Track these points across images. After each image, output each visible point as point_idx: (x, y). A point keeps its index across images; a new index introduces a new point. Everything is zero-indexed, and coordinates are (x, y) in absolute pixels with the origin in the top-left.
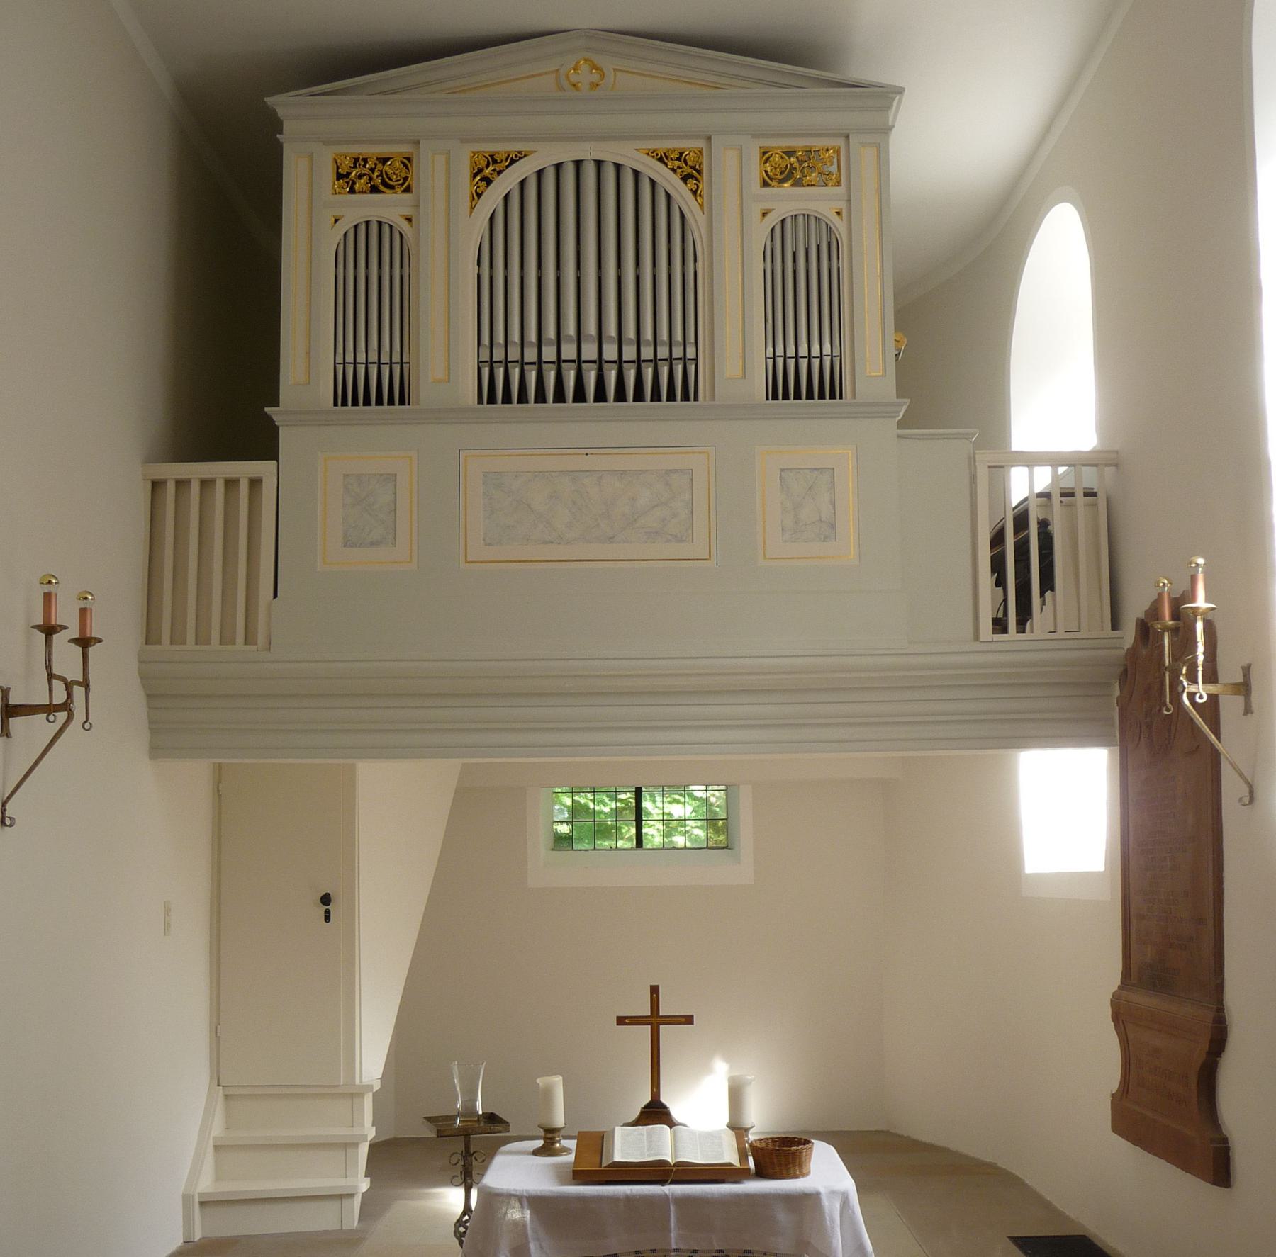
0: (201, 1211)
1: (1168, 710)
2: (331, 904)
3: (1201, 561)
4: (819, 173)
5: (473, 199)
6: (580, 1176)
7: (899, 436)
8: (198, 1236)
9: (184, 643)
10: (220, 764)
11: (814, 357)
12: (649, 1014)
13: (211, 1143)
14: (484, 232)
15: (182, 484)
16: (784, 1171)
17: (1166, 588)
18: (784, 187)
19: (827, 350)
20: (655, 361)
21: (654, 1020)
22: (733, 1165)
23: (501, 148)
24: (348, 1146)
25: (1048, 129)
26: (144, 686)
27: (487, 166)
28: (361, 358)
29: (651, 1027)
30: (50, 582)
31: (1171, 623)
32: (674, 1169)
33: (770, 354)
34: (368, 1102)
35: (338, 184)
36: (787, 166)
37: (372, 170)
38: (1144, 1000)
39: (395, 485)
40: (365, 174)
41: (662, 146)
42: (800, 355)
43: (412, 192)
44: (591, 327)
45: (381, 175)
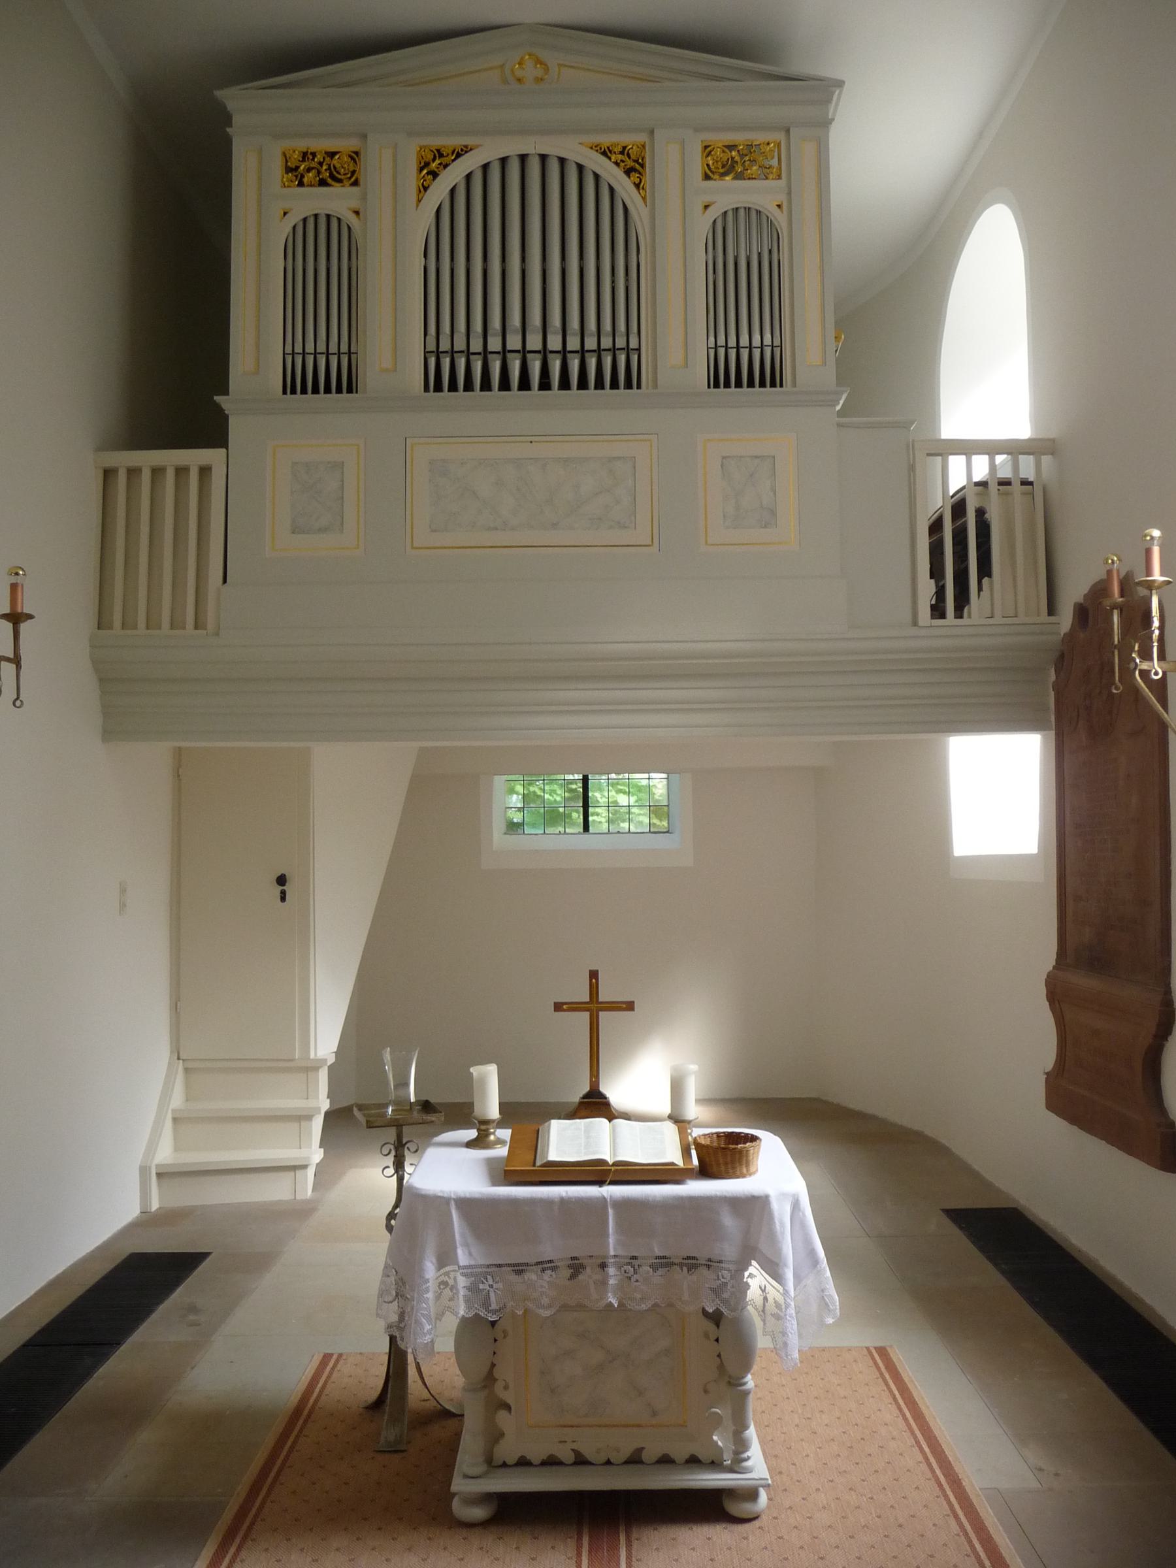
2: (287, 884)
3: (1156, 533)
4: (760, 167)
5: (420, 191)
7: (839, 425)
8: (155, 1206)
10: (179, 748)
11: (755, 347)
13: (169, 1116)
14: (430, 224)
15: (133, 472)
16: (731, 1171)
17: (1115, 565)
18: (725, 180)
19: (767, 340)
20: (599, 351)
21: (594, 1006)
22: (676, 1165)
27: (434, 160)
28: (310, 348)
30: (17, 574)
31: (1121, 599)
32: (613, 1168)
33: (712, 344)
34: (323, 1076)
35: (287, 178)
36: (728, 159)
37: (321, 164)
39: (343, 473)
40: (313, 168)
41: (606, 140)
43: (360, 185)
45: (329, 168)
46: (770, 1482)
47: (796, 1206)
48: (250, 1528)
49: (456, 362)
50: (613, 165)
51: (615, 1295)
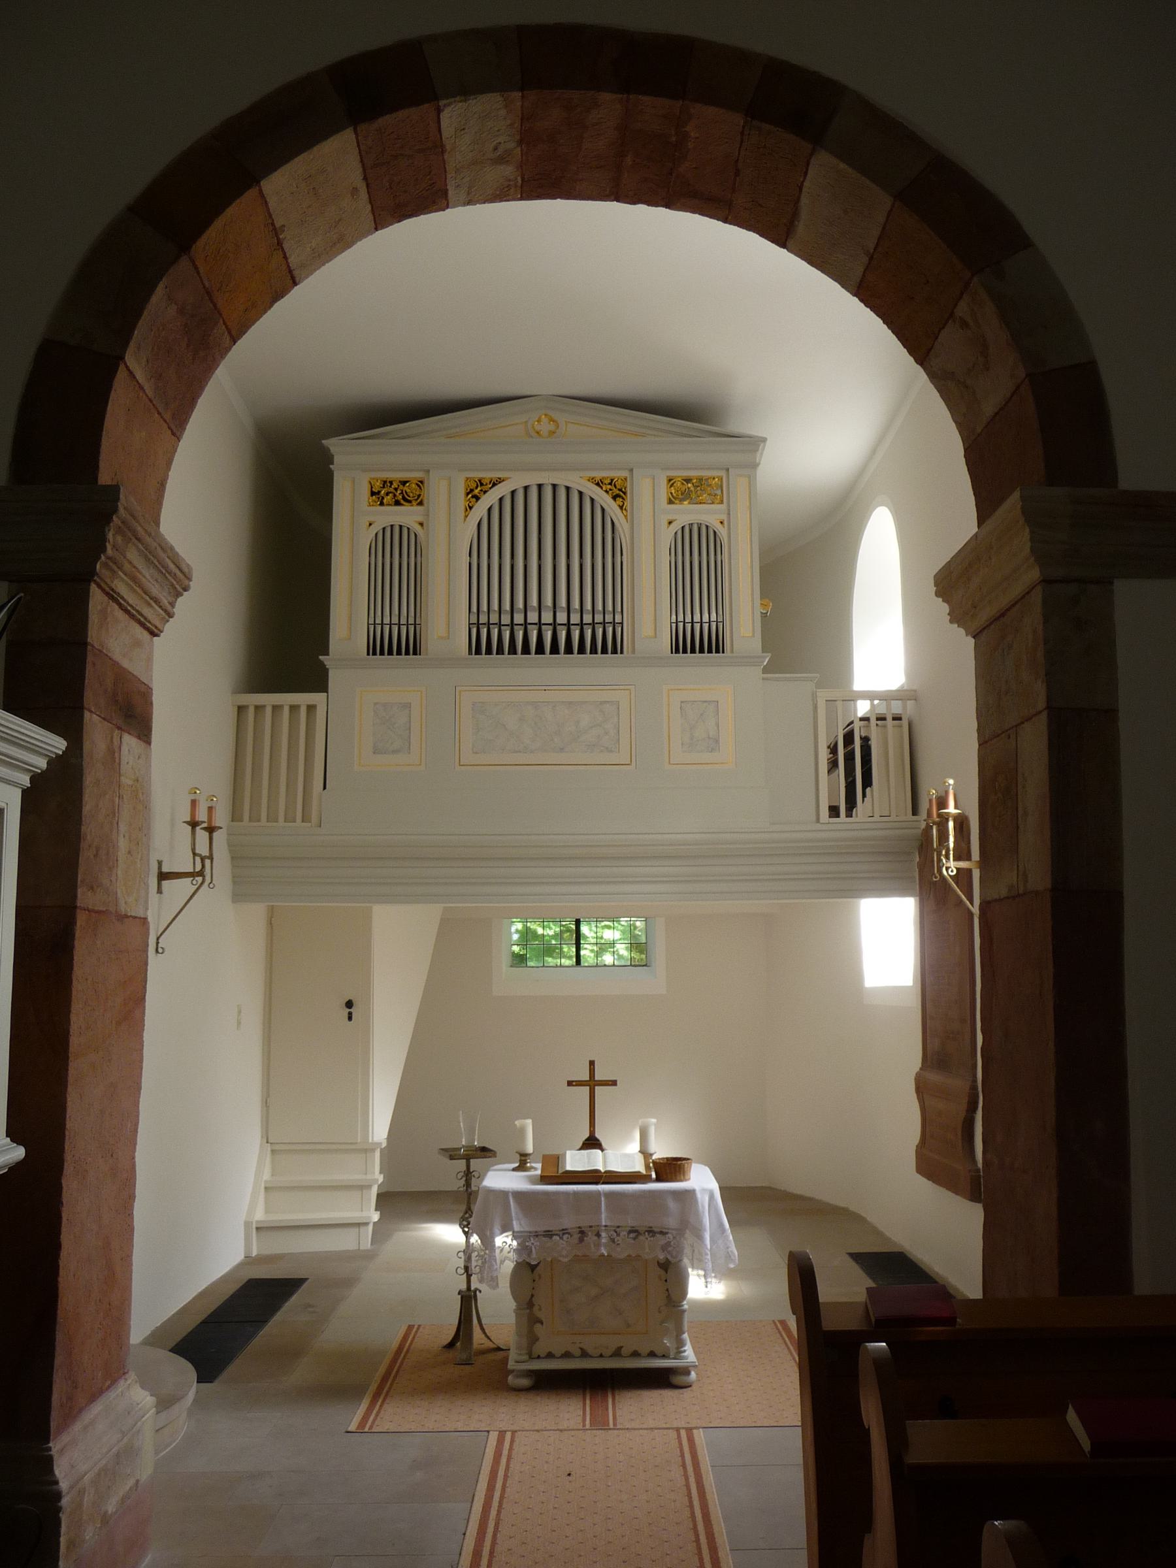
0: (257, 1236)
1: (936, 878)
2: (353, 1008)
3: (951, 782)
5: (467, 510)
6: (544, 1179)
7: (763, 679)
8: (254, 1254)
9: (259, 821)
10: (273, 906)
12: (588, 1079)
13: (263, 1186)
15: (259, 709)
23: (487, 475)
24: (364, 1187)
25: (874, 452)
26: (230, 851)
27: (477, 488)
29: (590, 1089)
31: (937, 819)
34: (377, 1154)
37: (396, 489)
38: (934, 1077)
39: (410, 711)
40: (391, 492)
41: (598, 475)
42: (695, 621)
44: (548, 600)
45: (402, 493)
46: (697, 1364)
47: (712, 1197)
48: (388, 1392)
49: (491, 633)
50: (604, 492)
51: (605, 1248)
